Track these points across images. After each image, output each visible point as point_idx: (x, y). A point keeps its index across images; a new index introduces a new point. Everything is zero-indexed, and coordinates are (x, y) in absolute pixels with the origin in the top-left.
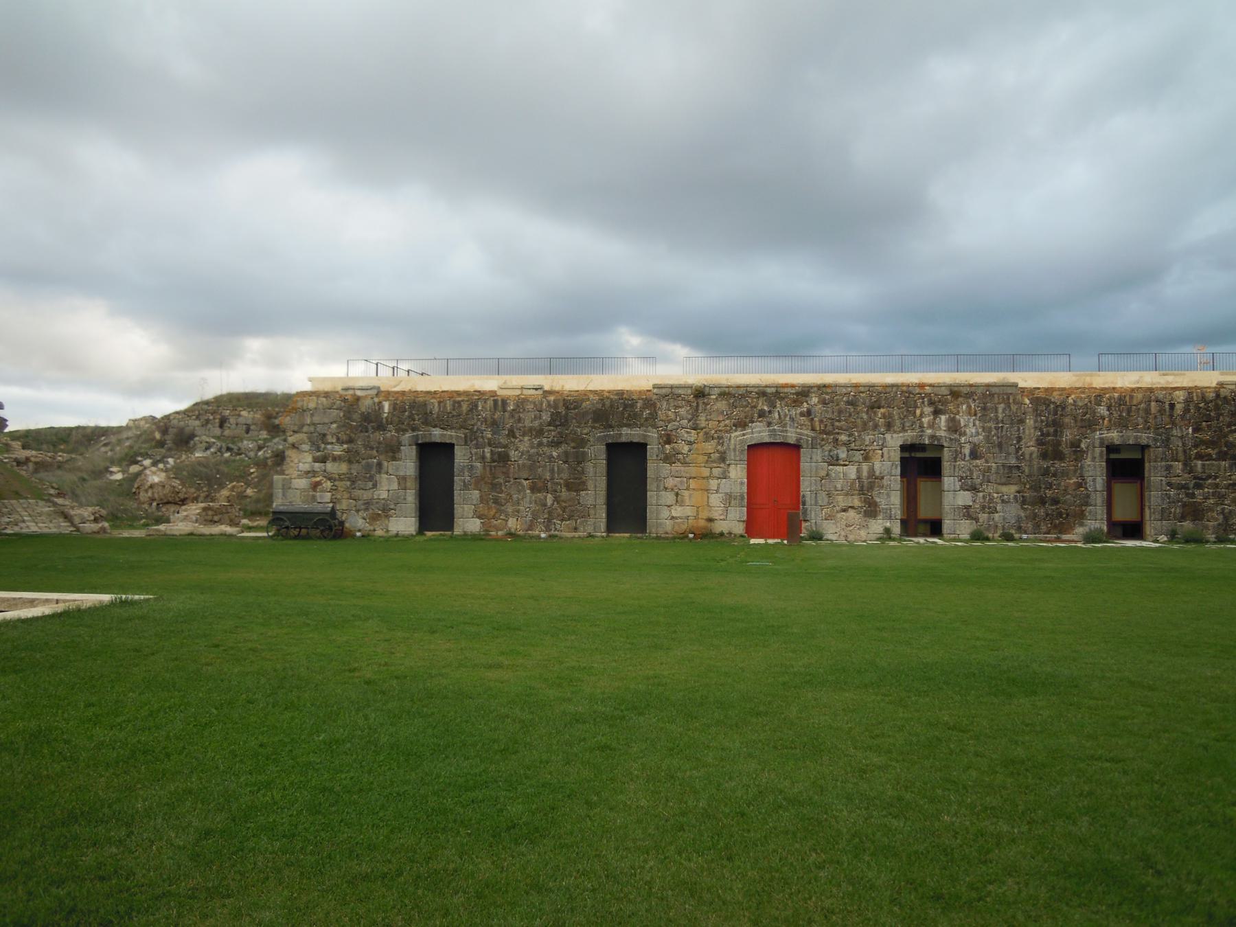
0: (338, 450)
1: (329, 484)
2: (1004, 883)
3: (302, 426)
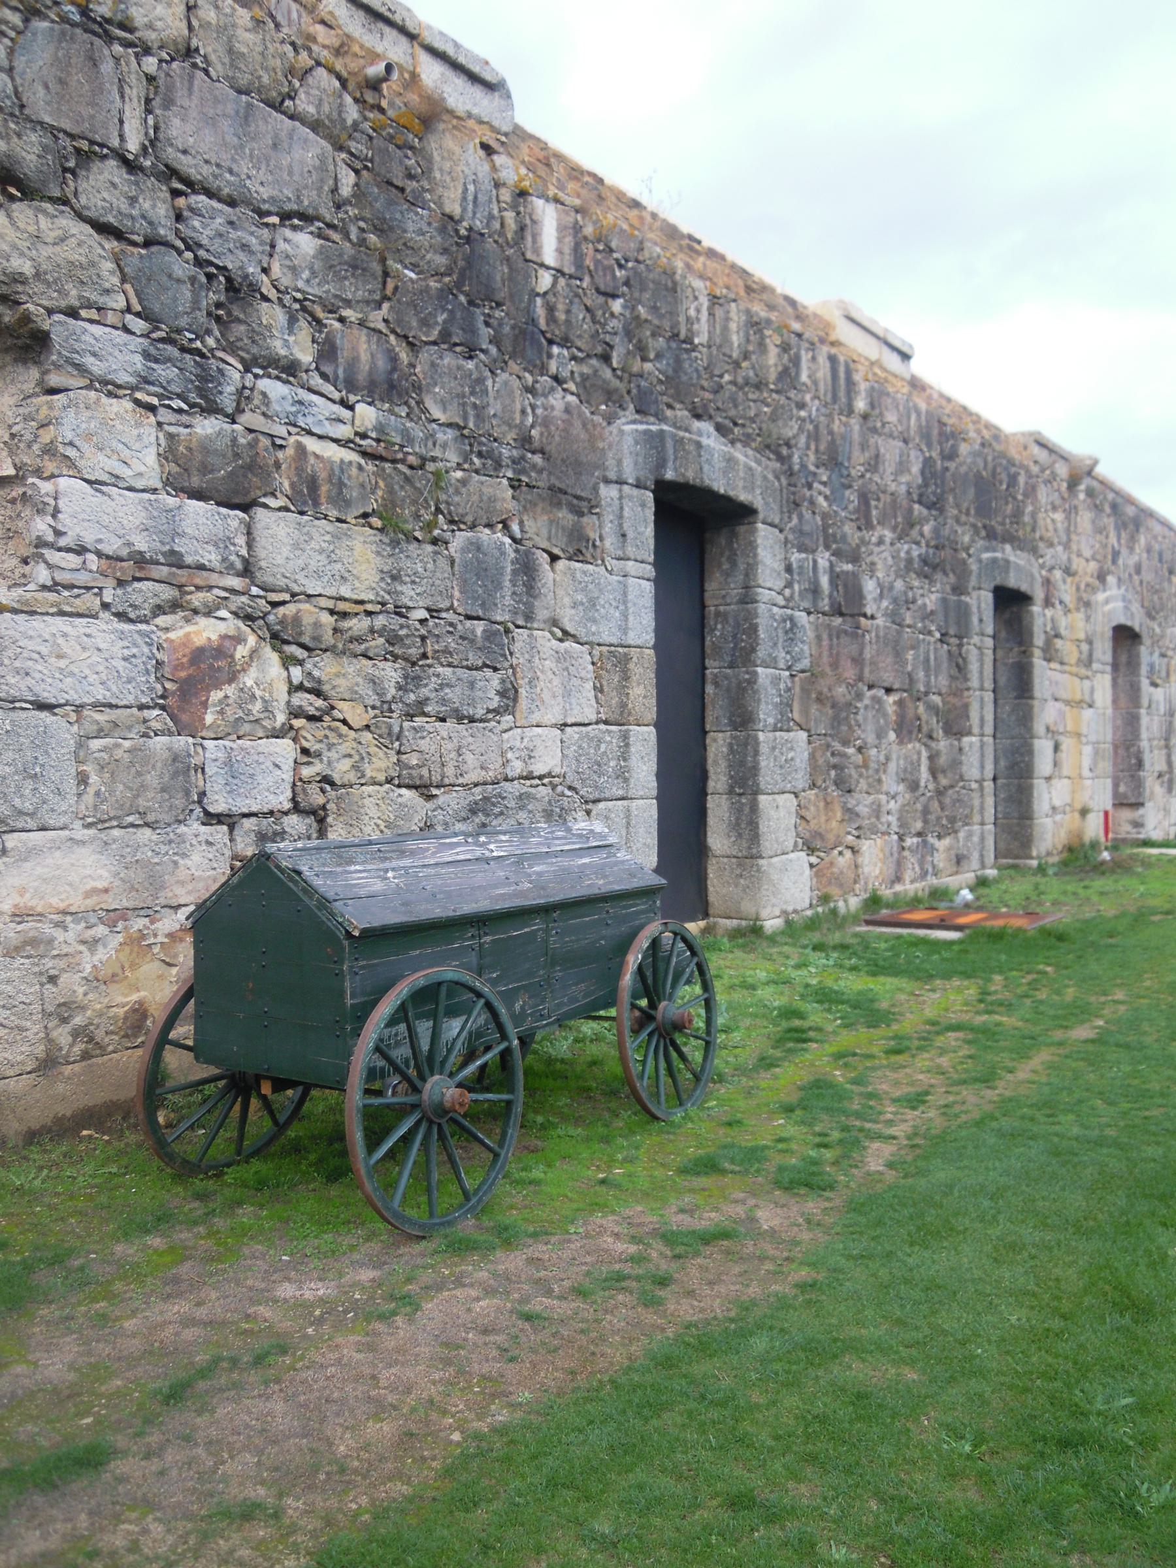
0: (326, 428)
1: (267, 676)
2: (121, 1136)
3: (88, 154)
